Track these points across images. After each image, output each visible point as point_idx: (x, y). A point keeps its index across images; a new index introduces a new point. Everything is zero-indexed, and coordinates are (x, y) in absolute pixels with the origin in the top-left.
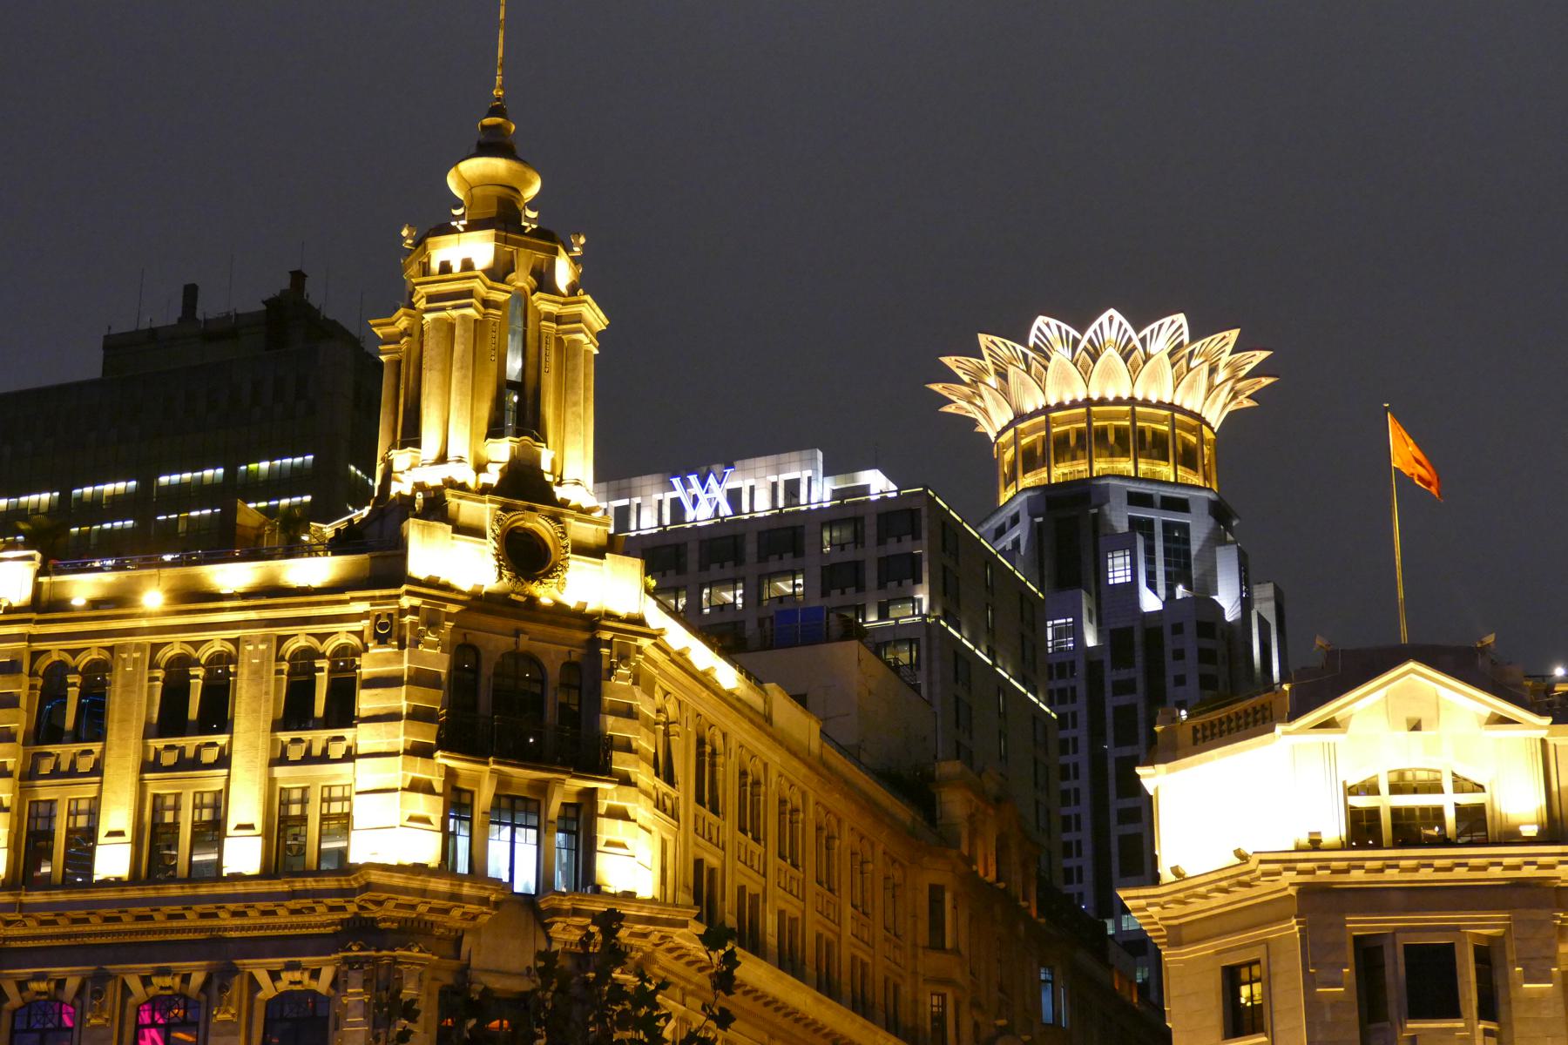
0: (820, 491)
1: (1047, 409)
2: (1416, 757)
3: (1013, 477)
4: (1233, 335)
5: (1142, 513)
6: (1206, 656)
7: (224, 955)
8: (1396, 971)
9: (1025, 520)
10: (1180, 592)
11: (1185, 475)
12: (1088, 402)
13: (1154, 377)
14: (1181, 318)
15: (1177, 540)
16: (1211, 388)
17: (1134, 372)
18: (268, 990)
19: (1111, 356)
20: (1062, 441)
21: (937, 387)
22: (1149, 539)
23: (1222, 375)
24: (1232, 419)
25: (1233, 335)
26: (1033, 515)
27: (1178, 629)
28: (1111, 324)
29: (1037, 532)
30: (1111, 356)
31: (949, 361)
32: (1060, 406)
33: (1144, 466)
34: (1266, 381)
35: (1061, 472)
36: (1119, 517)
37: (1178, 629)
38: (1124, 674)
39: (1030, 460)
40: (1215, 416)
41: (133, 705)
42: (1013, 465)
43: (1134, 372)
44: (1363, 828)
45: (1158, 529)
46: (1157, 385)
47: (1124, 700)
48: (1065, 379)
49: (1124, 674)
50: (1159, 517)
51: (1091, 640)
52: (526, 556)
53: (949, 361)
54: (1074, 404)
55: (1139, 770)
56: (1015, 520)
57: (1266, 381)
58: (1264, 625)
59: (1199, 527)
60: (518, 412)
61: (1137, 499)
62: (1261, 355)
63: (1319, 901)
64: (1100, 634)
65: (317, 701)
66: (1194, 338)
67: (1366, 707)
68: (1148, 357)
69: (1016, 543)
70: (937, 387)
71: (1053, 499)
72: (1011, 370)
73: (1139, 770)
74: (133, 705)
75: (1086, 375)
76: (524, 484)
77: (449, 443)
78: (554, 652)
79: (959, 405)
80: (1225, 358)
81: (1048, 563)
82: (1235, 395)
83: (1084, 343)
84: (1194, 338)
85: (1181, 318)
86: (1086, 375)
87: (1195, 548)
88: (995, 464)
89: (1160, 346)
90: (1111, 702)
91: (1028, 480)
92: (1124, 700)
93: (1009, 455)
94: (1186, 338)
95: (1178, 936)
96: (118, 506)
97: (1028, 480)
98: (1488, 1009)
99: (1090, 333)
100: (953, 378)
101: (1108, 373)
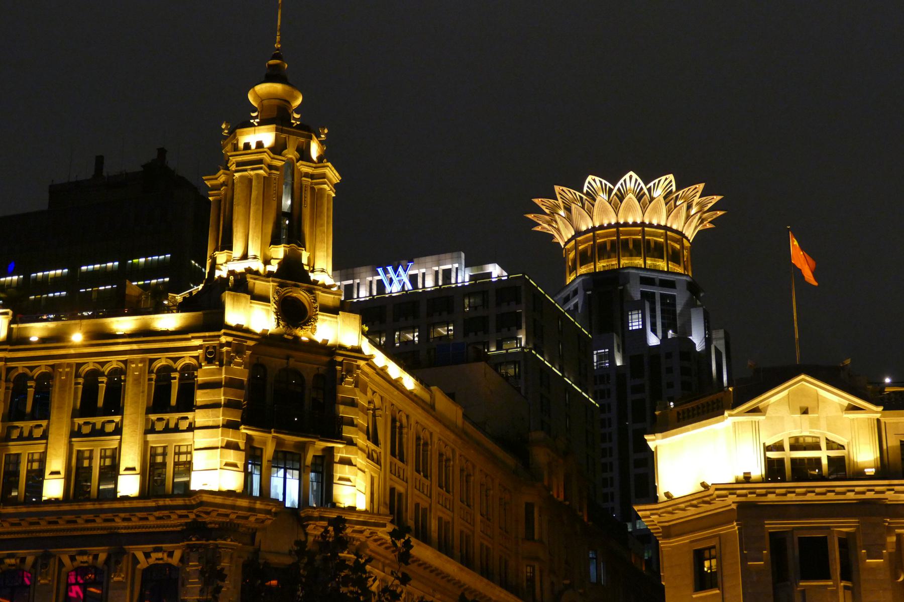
0: (464, 277)
1: (594, 229)
2: (803, 428)
4: (701, 186)
8: (793, 552)
9: (581, 292)
12: (617, 225)
14: (671, 177)
16: (688, 217)
18: (143, 563)
20: (603, 246)
21: (531, 216)
23: (693, 211)
25: (701, 186)
26: (585, 290)
28: (631, 180)
29: (588, 300)
31: (537, 201)
32: (601, 227)
33: (649, 262)
34: (720, 213)
35: (601, 265)
36: (636, 291)
39: (584, 258)
40: (690, 233)
43: (644, 208)
44: (774, 469)
45: (658, 298)
47: (638, 396)
50: (658, 291)
51: (619, 363)
52: (293, 313)
53: (537, 201)
56: (575, 292)
59: (681, 298)
61: (645, 281)
62: (717, 198)
64: (624, 359)
65: (172, 397)
68: (652, 199)
69: (576, 306)
70: (531, 216)
75: (616, 209)
76: (292, 272)
77: (247, 252)
82: (702, 220)
84: (678, 188)
86: (616, 209)
87: (679, 309)
89: (658, 193)
92: (638, 396)
93: (572, 255)
95: (669, 532)
96: (57, 284)
97: (583, 270)
98: (846, 574)
101: (629, 209)
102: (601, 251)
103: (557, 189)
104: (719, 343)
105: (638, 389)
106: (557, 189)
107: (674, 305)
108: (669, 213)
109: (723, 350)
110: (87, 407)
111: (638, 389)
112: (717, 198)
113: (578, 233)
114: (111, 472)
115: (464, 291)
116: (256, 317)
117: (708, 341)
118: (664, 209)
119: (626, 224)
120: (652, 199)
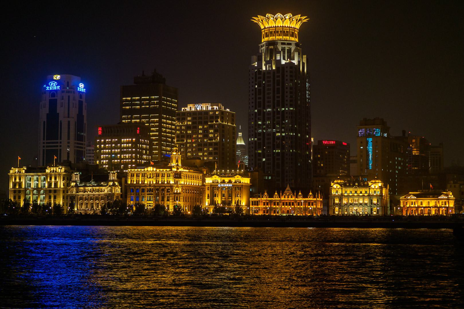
0: (210, 108)
1: (269, 27)
5: (283, 46)
6: (291, 72)
7: (165, 187)
12: (276, 27)
13: (287, 22)
15: (289, 51)
17: (283, 22)
19: (279, 19)
20: (271, 33)
27: (287, 67)
28: (279, 15)
30: (279, 19)
32: (271, 27)
33: (284, 37)
36: (280, 47)
37: (287, 67)
38: (278, 74)
40: (298, 27)
41: (160, 176)
43: (283, 22)
44: (213, 182)
46: (287, 24)
47: (278, 79)
48: (272, 23)
49: (278, 74)
51: (274, 68)
52: (178, 169)
54: (273, 27)
58: (303, 64)
59: (293, 48)
60: (177, 161)
63: (211, 185)
64: (276, 67)
65: (169, 176)
67: (213, 177)
68: (286, 19)
74: (160, 176)
75: (275, 22)
76: (177, 165)
77: (174, 164)
86: (275, 22)
89: (287, 17)
90: (276, 79)
91: (266, 39)
92: (278, 79)
96: (138, 100)
101: (279, 22)
105: (278, 77)
108: (291, 23)
110: (162, 176)
111: (278, 77)
113: (265, 28)
114: (164, 181)
115: (210, 111)
116: (174, 169)
118: (289, 22)
119: (278, 27)
120: (286, 19)
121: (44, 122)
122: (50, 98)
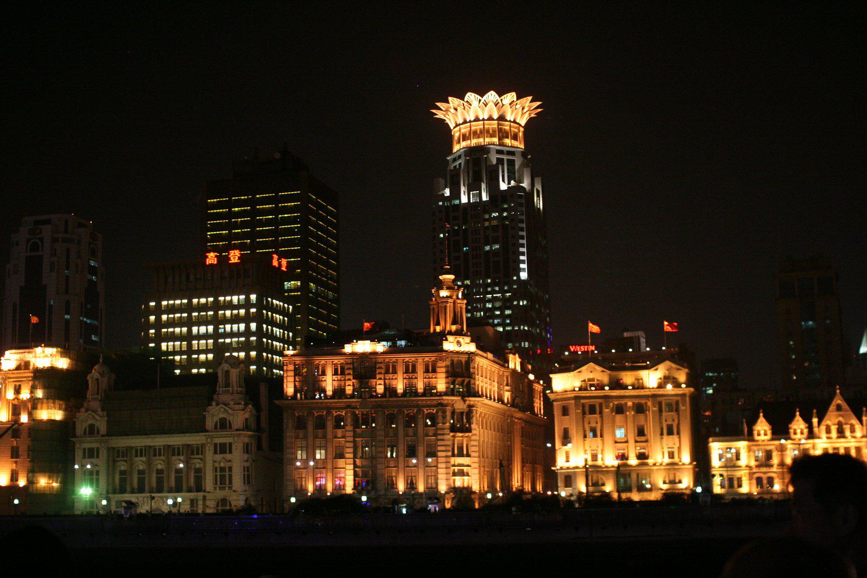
2: (591, 376)
3: (459, 142)
4: (530, 98)
8: (587, 409)
9: (463, 157)
10: (513, 183)
11: (516, 143)
14: (514, 94)
16: (523, 114)
18: (426, 412)
20: (475, 133)
21: (434, 111)
22: (503, 165)
23: (525, 110)
24: (530, 121)
25: (530, 98)
26: (466, 156)
29: (467, 162)
31: (438, 104)
34: (539, 110)
35: (474, 142)
39: (465, 138)
42: (459, 139)
45: (505, 162)
50: (505, 157)
53: (438, 104)
55: (551, 376)
56: (460, 157)
57: (539, 110)
61: (498, 152)
62: (539, 103)
66: (518, 99)
69: (460, 164)
70: (434, 111)
71: (470, 151)
72: (459, 109)
73: (551, 376)
78: (464, 359)
79: (440, 115)
80: (528, 104)
81: (471, 173)
82: (530, 114)
83: (483, 101)
84: (518, 99)
85: (514, 94)
87: (517, 167)
88: (451, 137)
91: (464, 144)
93: (457, 135)
94: (515, 99)
95: (556, 400)
97: (464, 144)
98: (601, 436)
99: (485, 97)
100: (440, 109)
102: (476, 134)
103: (450, 99)
104: (538, 186)
106: (450, 99)
107: (514, 165)
109: (540, 189)
112: (539, 103)
117: (533, 184)
121: (15, 305)
122: (28, 254)
